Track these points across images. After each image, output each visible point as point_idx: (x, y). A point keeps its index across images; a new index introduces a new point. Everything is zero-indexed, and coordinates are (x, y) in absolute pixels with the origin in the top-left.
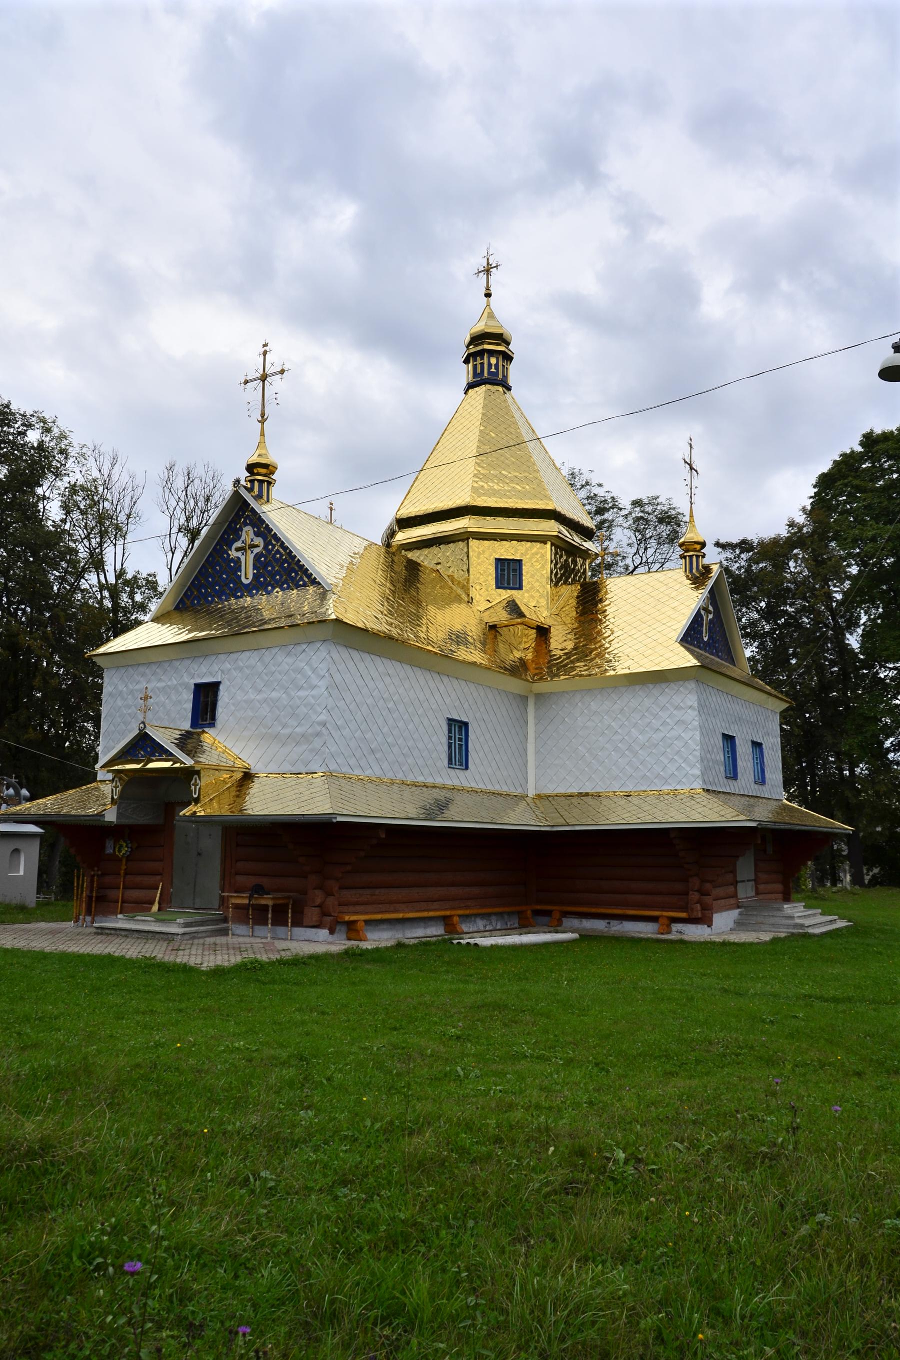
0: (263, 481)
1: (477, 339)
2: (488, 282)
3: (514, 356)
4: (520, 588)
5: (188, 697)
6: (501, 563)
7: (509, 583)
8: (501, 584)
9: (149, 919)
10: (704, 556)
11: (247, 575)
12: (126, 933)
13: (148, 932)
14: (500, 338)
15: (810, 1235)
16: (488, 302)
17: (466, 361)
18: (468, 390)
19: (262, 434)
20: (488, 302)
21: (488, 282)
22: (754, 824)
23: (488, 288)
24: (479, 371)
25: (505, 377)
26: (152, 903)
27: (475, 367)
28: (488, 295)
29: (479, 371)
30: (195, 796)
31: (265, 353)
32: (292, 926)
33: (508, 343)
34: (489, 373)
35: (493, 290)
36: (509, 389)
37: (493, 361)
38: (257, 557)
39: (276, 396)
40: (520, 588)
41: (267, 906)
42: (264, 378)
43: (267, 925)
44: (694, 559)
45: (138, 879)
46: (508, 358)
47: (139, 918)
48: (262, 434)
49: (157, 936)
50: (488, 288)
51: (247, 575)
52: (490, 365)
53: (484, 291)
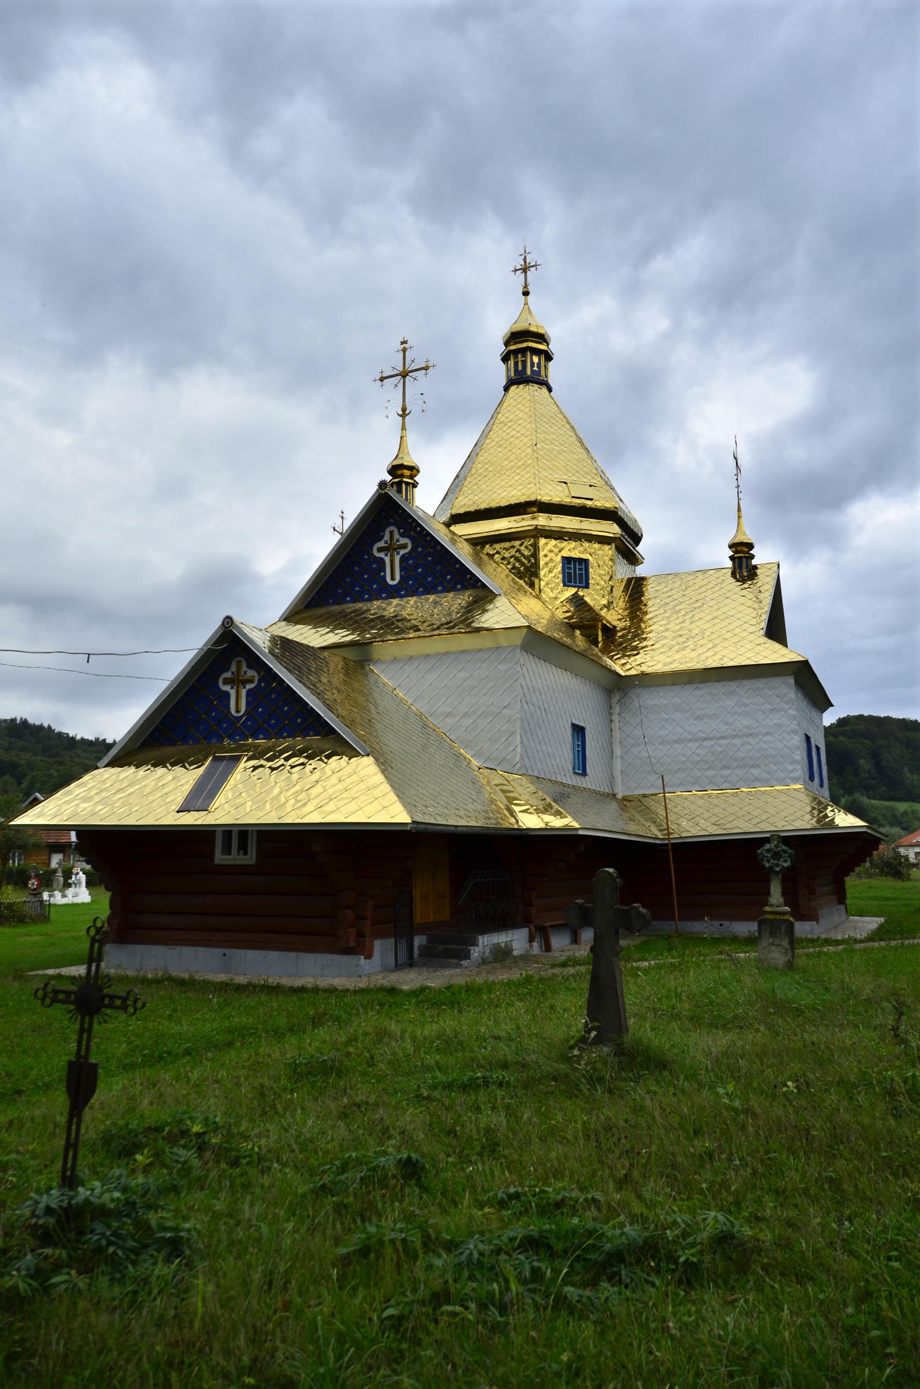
0: (409, 483)
1: (516, 336)
2: (526, 280)
4: (587, 586)
5: (582, 724)
6: (567, 560)
7: (575, 582)
8: (568, 580)
10: (753, 557)
11: (393, 577)
14: (541, 338)
15: (700, 1155)
16: (526, 300)
17: (505, 359)
18: (506, 389)
20: (526, 300)
21: (526, 280)
23: (526, 286)
27: (516, 364)
31: (404, 350)
34: (532, 371)
35: (530, 288)
37: (536, 359)
38: (403, 559)
40: (587, 586)
42: (404, 375)
44: (744, 560)
46: (549, 357)
50: (526, 286)
51: (393, 577)
53: (521, 290)
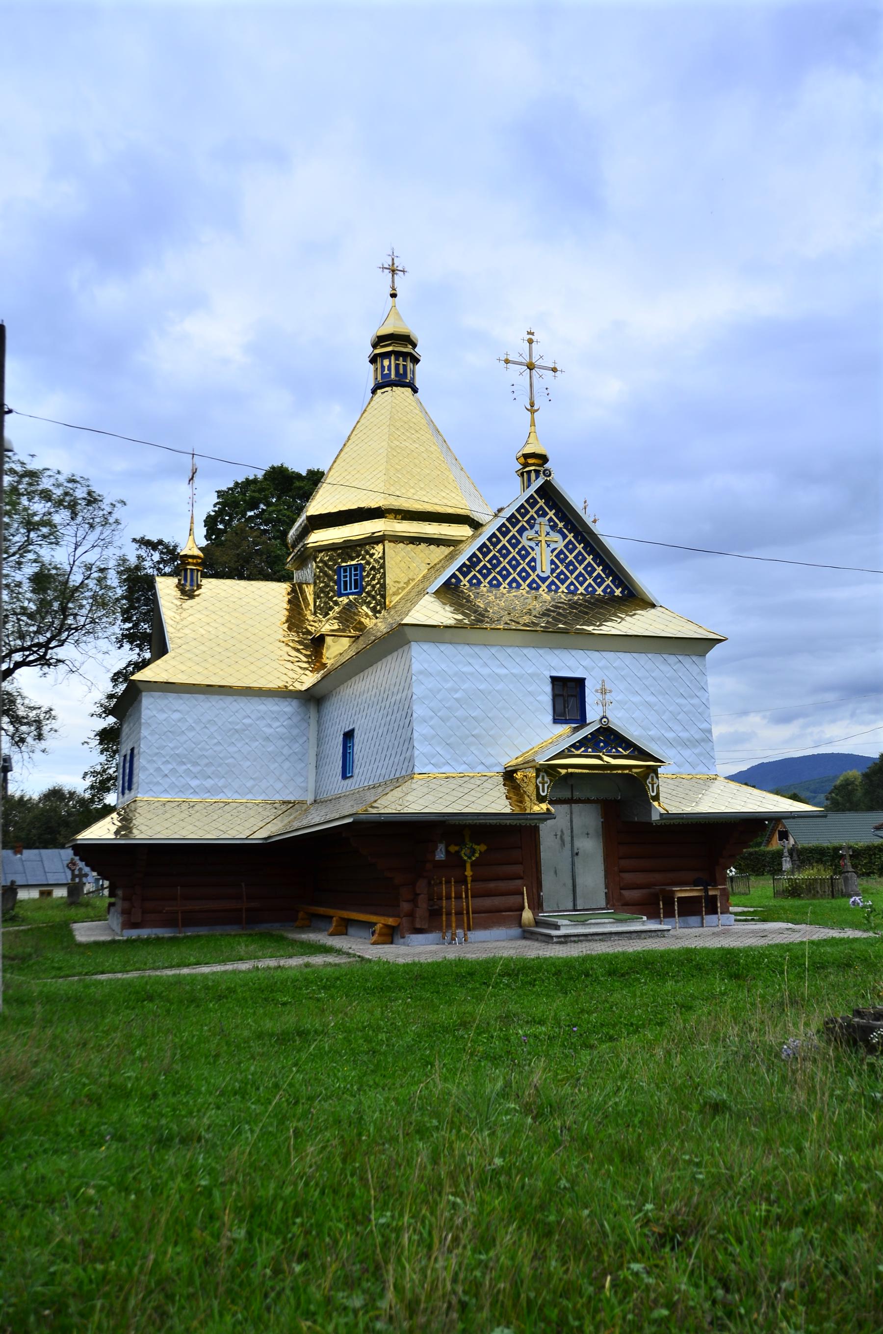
1: (380, 340)
2: (393, 282)
3: (421, 359)
9: (606, 921)
12: (601, 937)
13: (631, 932)
14: (406, 339)
19: (533, 424)
21: (393, 282)
22: (350, 820)
24: (401, 371)
25: (413, 379)
26: (522, 909)
28: (394, 296)
29: (401, 371)
30: (654, 794)
32: (664, 917)
33: (414, 345)
36: (415, 391)
37: (386, 363)
39: (513, 388)
41: (716, 896)
42: (531, 367)
43: (674, 917)
45: (492, 885)
47: (593, 921)
48: (533, 424)
49: (643, 935)
52: (397, 366)
53: (390, 291)
